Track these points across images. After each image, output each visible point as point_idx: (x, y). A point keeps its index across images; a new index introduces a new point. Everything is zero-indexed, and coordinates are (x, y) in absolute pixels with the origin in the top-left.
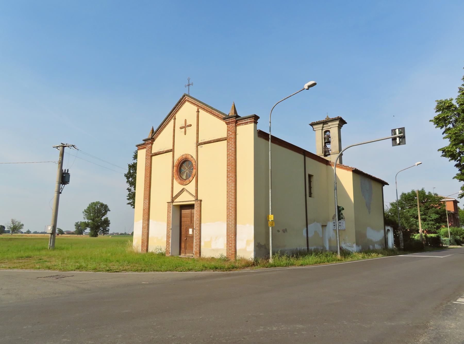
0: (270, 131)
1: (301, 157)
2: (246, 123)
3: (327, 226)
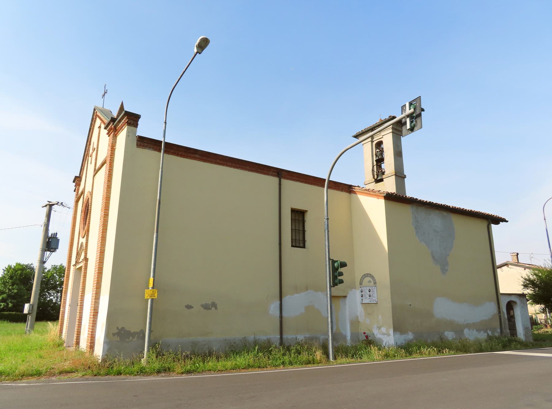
0: (164, 137)
1: (274, 180)
3: (348, 297)
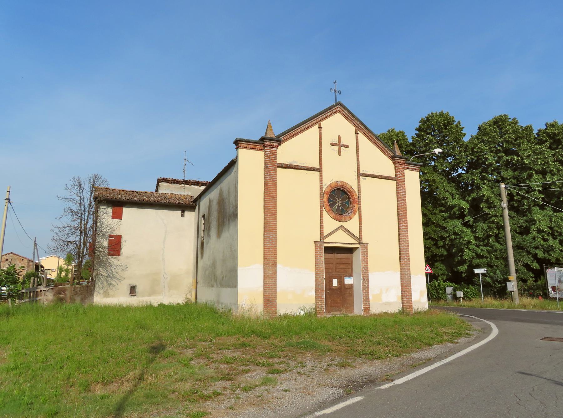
2: (412, 170)
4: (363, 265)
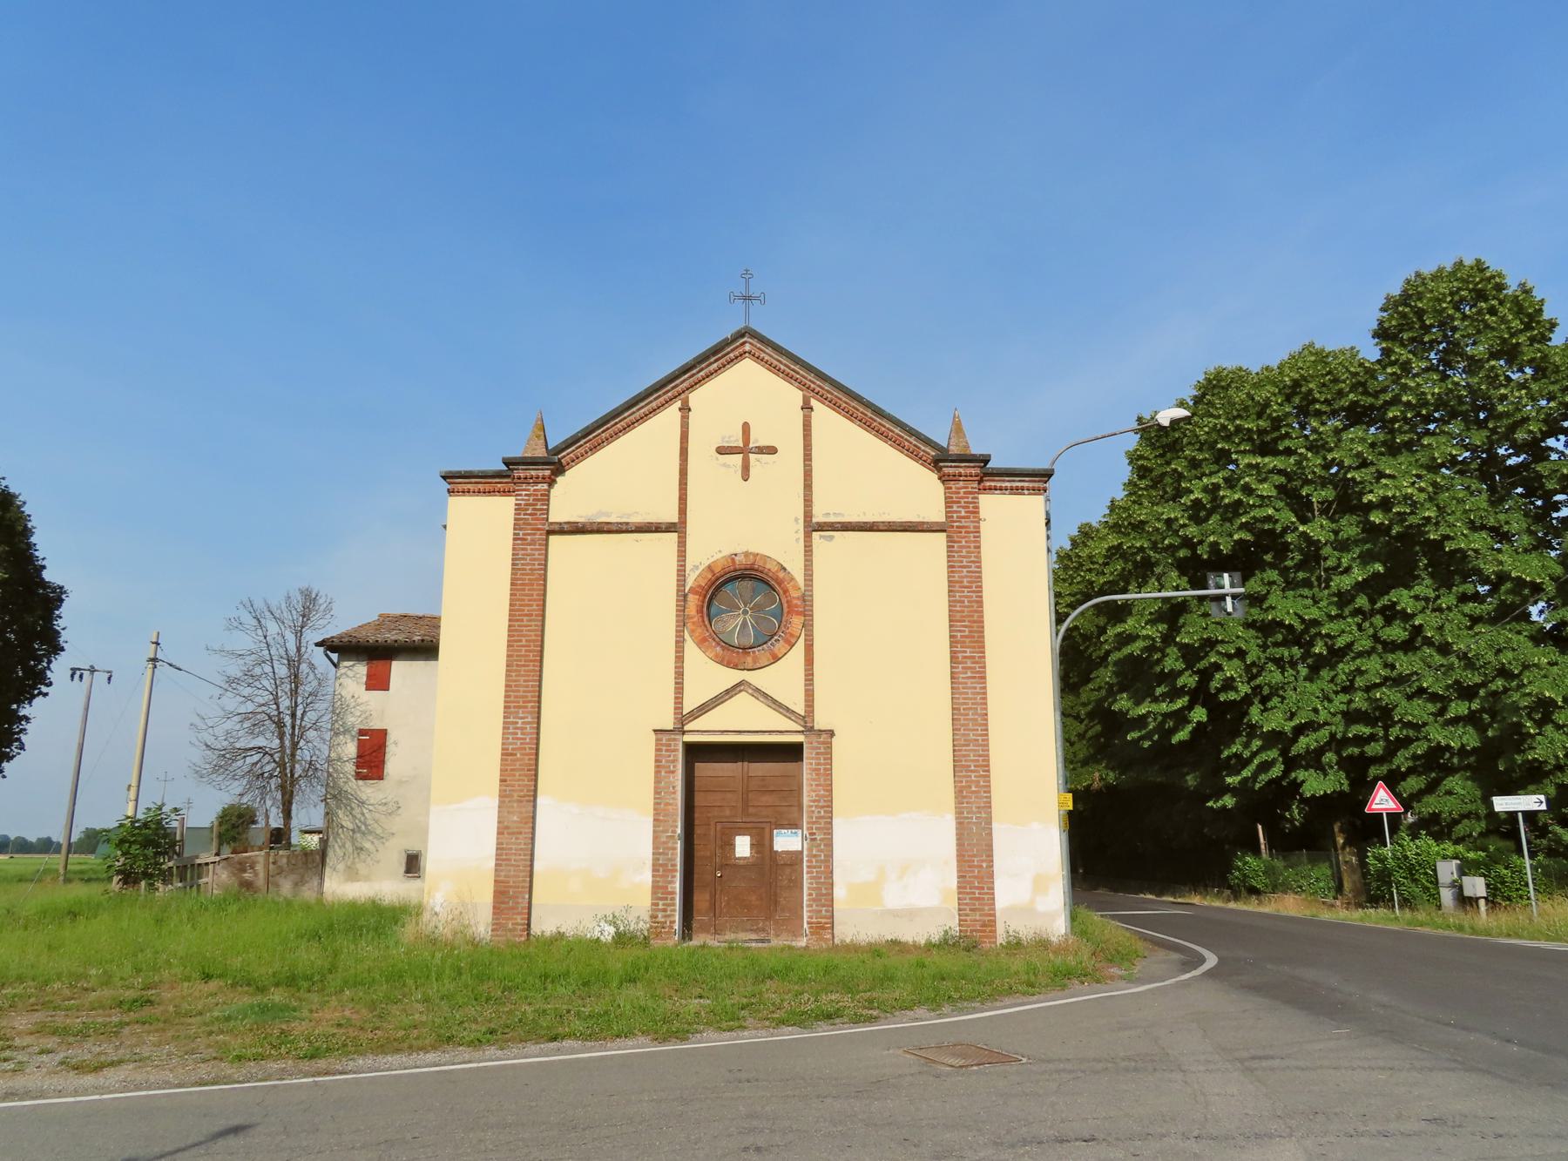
4: (814, 794)
